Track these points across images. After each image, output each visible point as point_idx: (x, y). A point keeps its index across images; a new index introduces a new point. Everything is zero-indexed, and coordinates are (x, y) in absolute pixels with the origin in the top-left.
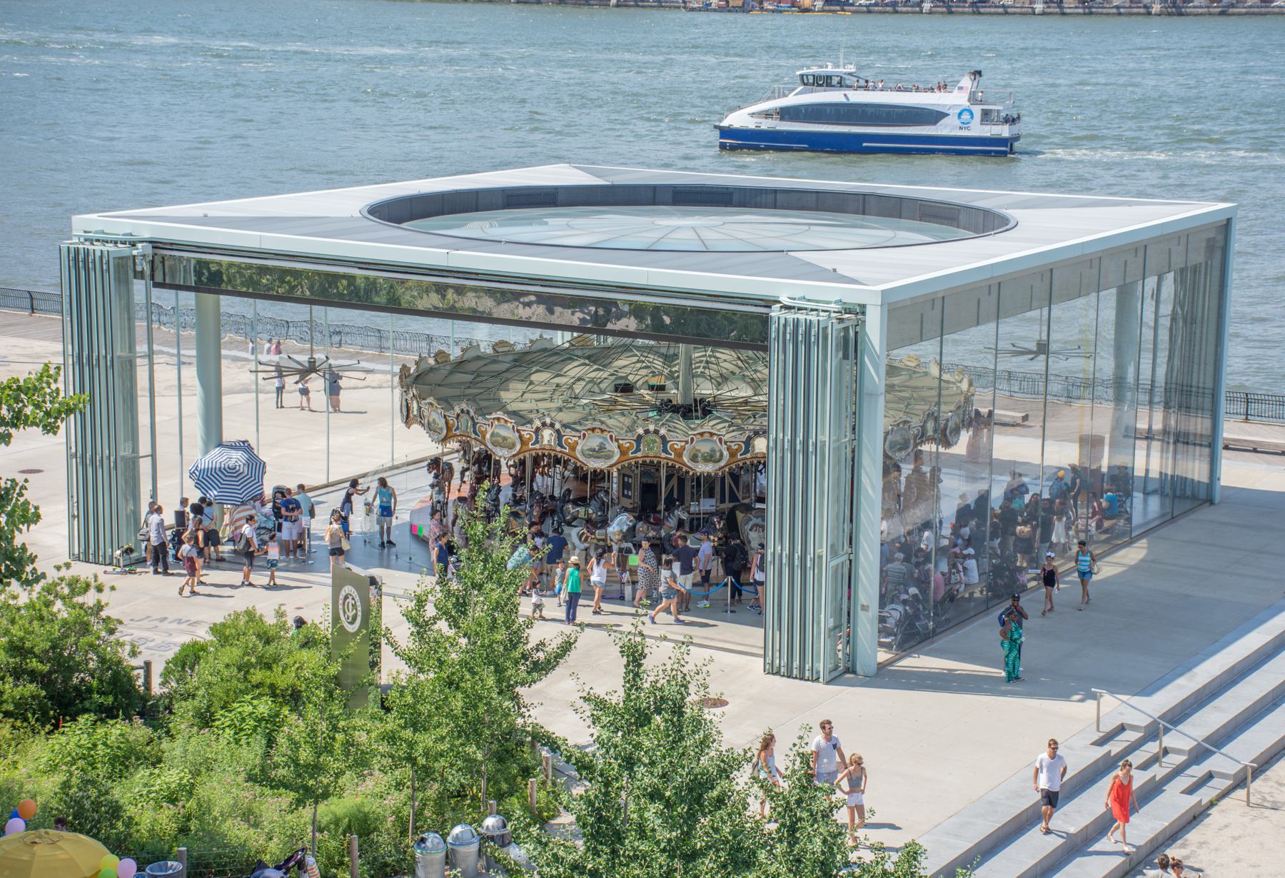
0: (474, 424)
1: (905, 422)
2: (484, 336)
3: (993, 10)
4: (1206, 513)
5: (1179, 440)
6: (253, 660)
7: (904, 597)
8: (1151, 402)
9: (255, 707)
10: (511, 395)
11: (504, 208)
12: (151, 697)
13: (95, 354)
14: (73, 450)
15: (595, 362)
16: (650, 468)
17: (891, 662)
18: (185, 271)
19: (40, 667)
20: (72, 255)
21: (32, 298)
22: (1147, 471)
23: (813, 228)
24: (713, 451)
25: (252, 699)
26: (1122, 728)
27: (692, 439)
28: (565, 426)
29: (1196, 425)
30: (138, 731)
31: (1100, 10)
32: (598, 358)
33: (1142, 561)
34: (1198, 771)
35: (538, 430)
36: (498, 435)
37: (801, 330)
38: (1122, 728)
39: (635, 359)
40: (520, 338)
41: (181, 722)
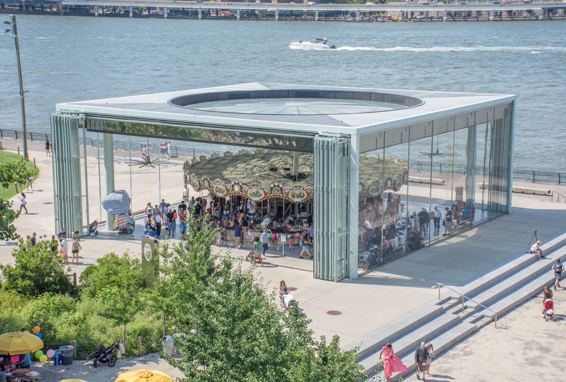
0: (209, 184)
1: (377, 181)
2: (224, 149)
3: (472, 19)
4: (505, 218)
5: (496, 189)
6: (112, 272)
7: (371, 249)
8: (484, 174)
9: (111, 290)
10: (227, 173)
11: (228, 99)
12: (76, 286)
13: (64, 157)
14: (56, 194)
15: (264, 160)
16: (279, 200)
17: (364, 274)
18: (99, 125)
19: (31, 274)
20: (55, 119)
21: (32, 135)
22: (483, 201)
23: (345, 106)
24: (301, 193)
25: (110, 286)
26: (450, 298)
27: (292, 189)
28: (244, 184)
29: (502, 182)
30: (67, 299)
31: (517, 19)
32: (265, 158)
33: (473, 236)
34: (478, 315)
35: (233, 185)
36: (218, 188)
37: (325, 144)
38: (450, 298)
39: (279, 158)
40: (235, 150)
41: (84, 296)
